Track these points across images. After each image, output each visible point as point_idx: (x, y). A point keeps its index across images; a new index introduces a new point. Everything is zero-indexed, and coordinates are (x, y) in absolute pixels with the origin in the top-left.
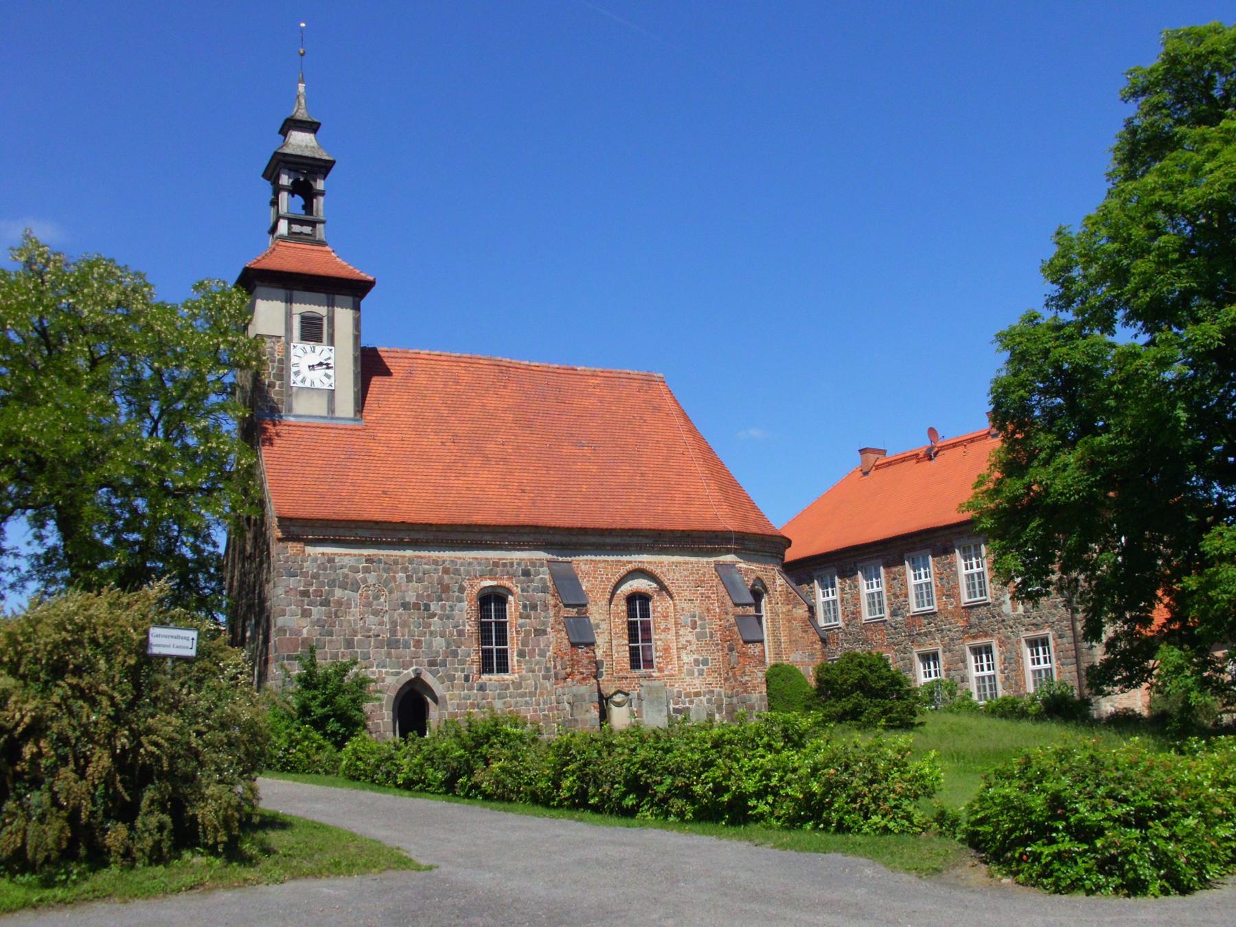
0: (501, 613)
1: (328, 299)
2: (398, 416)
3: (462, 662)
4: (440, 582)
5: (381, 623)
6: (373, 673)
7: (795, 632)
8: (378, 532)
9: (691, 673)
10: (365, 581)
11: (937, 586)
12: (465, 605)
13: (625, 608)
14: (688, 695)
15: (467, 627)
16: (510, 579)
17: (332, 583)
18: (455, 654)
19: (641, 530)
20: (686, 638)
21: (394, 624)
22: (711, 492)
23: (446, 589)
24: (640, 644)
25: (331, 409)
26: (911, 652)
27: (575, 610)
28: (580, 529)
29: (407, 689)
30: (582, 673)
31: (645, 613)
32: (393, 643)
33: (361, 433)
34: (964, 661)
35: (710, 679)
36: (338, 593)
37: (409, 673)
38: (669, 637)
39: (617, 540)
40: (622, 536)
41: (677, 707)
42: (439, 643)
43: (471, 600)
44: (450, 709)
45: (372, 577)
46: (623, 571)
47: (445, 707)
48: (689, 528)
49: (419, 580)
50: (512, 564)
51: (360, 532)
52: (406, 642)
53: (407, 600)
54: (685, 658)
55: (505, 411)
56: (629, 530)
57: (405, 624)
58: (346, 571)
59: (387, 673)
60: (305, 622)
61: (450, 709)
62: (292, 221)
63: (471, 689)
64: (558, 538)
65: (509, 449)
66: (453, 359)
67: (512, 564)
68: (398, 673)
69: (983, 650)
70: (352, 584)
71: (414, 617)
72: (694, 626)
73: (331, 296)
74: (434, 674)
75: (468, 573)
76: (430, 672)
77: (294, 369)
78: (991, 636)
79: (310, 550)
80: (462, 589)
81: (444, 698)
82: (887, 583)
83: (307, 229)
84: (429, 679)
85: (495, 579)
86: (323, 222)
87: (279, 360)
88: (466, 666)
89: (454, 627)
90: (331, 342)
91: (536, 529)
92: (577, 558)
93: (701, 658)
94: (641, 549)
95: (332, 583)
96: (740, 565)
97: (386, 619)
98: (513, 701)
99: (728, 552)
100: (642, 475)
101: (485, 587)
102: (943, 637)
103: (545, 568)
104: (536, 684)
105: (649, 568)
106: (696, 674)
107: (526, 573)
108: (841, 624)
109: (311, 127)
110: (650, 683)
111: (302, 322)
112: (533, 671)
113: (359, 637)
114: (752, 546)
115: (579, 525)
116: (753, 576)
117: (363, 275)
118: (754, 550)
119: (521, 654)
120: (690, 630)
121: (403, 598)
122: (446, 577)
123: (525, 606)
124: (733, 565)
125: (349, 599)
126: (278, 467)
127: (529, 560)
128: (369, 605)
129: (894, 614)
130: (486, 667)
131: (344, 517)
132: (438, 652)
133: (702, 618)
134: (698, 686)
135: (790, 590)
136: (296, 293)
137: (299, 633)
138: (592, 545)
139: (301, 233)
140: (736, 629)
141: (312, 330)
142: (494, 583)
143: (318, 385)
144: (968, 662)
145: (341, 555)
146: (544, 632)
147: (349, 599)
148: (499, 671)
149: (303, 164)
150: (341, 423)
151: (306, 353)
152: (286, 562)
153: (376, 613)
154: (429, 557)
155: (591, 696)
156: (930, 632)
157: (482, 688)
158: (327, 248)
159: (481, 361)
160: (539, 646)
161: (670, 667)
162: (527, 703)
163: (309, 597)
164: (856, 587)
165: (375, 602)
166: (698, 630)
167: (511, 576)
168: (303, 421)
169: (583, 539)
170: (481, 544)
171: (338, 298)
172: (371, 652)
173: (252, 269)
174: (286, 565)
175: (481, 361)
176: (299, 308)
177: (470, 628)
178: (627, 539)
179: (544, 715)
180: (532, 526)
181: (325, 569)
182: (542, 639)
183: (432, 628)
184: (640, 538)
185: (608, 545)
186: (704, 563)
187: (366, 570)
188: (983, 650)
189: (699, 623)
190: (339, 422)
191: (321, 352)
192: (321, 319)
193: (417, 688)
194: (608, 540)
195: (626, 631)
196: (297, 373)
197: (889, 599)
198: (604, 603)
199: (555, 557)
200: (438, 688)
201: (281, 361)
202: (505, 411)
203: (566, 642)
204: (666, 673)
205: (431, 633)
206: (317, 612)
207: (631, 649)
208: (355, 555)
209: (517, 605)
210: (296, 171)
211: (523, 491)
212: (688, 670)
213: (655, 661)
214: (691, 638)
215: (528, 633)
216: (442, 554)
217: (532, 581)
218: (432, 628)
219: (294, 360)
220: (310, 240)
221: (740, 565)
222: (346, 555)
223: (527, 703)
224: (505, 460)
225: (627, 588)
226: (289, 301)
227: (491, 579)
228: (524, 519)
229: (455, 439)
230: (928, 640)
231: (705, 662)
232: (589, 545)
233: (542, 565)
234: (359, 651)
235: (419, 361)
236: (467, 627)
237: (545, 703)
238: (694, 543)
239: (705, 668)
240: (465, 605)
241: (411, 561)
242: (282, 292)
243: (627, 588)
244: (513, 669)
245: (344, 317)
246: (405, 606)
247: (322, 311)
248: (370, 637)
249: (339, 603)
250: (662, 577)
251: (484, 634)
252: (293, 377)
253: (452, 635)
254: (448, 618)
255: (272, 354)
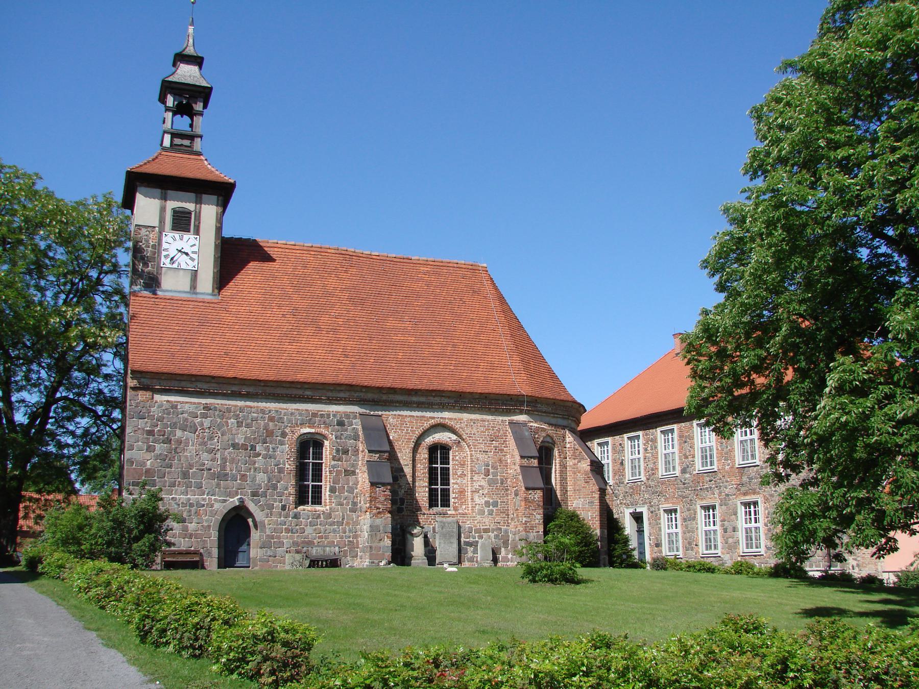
0: (318, 455)
1: (196, 197)
2: (250, 293)
3: (281, 495)
4: (266, 428)
5: (213, 460)
6: (204, 499)
7: (579, 483)
8: (215, 385)
9: (482, 512)
10: (202, 424)
11: (717, 449)
12: (286, 447)
13: (427, 456)
14: (478, 531)
15: (287, 466)
16: (327, 427)
17: (174, 426)
18: (275, 487)
19: (443, 391)
20: (479, 483)
21: (224, 460)
22: (513, 362)
23: (270, 433)
24: (439, 487)
25: (194, 286)
26: (695, 505)
27: (378, 455)
28: (389, 388)
29: (234, 513)
30: (378, 508)
31: (445, 460)
32: (222, 476)
33: (216, 306)
34: (735, 514)
35: (498, 519)
36: (179, 433)
37: (234, 501)
38: (465, 481)
39: (423, 399)
40: (427, 396)
41: (468, 540)
42: (261, 478)
43: (291, 444)
44: (268, 532)
45: (207, 423)
46: (426, 425)
47: (263, 531)
48: (487, 391)
49: (248, 426)
50: (329, 415)
51: (199, 385)
52: (234, 476)
53: (237, 441)
54: (477, 500)
55: (342, 290)
56: (433, 391)
57: (233, 461)
58: (185, 415)
59: (215, 500)
60: (148, 456)
61: (268, 532)
62: (174, 135)
63: (287, 516)
64: (370, 396)
65: (340, 321)
66: (305, 248)
67: (329, 415)
68: (225, 501)
69: (301, 483)
70: (191, 427)
71: (242, 455)
72: (487, 473)
73: (199, 195)
74: (256, 503)
75: (290, 421)
76: (252, 500)
77: (164, 253)
78: (759, 493)
79: (158, 397)
80: (284, 435)
81: (263, 523)
82: (680, 444)
83: (187, 142)
84: (252, 507)
85: (313, 427)
86: (201, 137)
87: (152, 245)
88: (284, 498)
89: (276, 465)
90: (197, 232)
91: (351, 387)
92: (387, 413)
93: (491, 501)
94: (443, 407)
95: (174, 426)
96: (531, 424)
97: (218, 456)
98: (322, 528)
99: (521, 412)
100: (454, 346)
101: (305, 434)
102: (720, 493)
103: (358, 421)
104: (343, 515)
105: (449, 423)
106: (486, 513)
107: (341, 423)
108: (643, 478)
109: (198, 61)
110: (444, 519)
111: (173, 216)
112: (342, 505)
113: (194, 470)
114: (544, 408)
115: (389, 385)
116: (544, 434)
117: (226, 178)
118: (545, 412)
119: (333, 490)
120: (483, 476)
121: (234, 439)
122: (271, 424)
123: (338, 450)
124: (524, 424)
125: (187, 439)
126: (140, 331)
127: (344, 412)
128: (205, 444)
129: (684, 471)
130: (301, 499)
131: (186, 372)
132: (260, 485)
133: (494, 467)
134: (487, 523)
135: (577, 446)
136: (170, 192)
137: (144, 464)
138: (400, 402)
139: (182, 145)
140: (520, 477)
141: (182, 222)
142: (313, 431)
143: (184, 266)
144: (739, 515)
145: (183, 403)
146: (354, 473)
147: (187, 439)
148: (313, 503)
149: (184, 90)
150: (200, 297)
151: (175, 240)
152: (137, 407)
153: (210, 451)
154: (257, 407)
155: (384, 527)
156: (711, 488)
157: (296, 516)
158: (202, 157)
159: (329, 251)
160: (348, 484)
161: (464, 507)
162: (334, 531)
163: (154, 436)
164: (656, 448)
165: (209, 442)
166: (491, 477)
167: (328, 426)
168: (168, 295)
169: (391, 397)
170: (295, 397)
171: (205, 197)
172: (204, 483)
173: (133, 172)
174: (136, 409)
175: (329, 251)
176: (171, 205)
177: (290, 466)
178: (432, 398)
179: (349, 541)
180: (346, 385)
181: (169, 414)
182: (352, 479)
183: (256, 465)
184: (443, 398)
185: (414, 403)
186: (500, 421)
187: (204, 416)
188: (301, 483)
189: (491, 471)
190: (167, 294)
191: (188, 241)
192: (190, 213)
193: (242, 513)
194: (415, 399)
195: (427, 475)
196: (166, 257)
197: (680, 459)
198: (408, 451)
199: (368, 411)
200: (259, 514)
201: (154, 246)
202: (342, 290)
203: (367, 481)
204: (460, 511)
205: (255, 469)
206: (160, 448)
207: (431, 490)
208: (195, 403)
209: (331, 450)
210: (180, 95)
211: (346, 356)
212: (479, 510)
213: (452, 500)
214: (483, 483)
215: (339, 473)
216: (268, 405)
217: (346, 430)
218: (256, 465)
219: (165, 246)
220: (190, 151)
221: (531, 424)
222: (187, 402)
223: (334, 531)
224: (335, 330)
225: (429, 440)
226: (164, 198)
227: (309, 427)
228: (342, 379)
229: (295, 312)
230: (709, 494)
231: (495, 504)
232: (397, 402)
233: (355, 417)
234: (193, 481)
235: (276, 249)
236: (287, 466)
237: (350, 531)
238: (491, 404)
239: (494, 509)
240: (286, 447)
241: (242, 410)
242: (158, 191)
243: (429, 440)
244: (325, 502)
245: (209, 212)
246: (235, 446)
247: (191, 206)
248: (203, 470)
249: (179, 442)
250: (461, 432)
251: (301, 472)
252: (163, 259)
253: (273, 472)
254: (270, 457)
255: (147, 241)
